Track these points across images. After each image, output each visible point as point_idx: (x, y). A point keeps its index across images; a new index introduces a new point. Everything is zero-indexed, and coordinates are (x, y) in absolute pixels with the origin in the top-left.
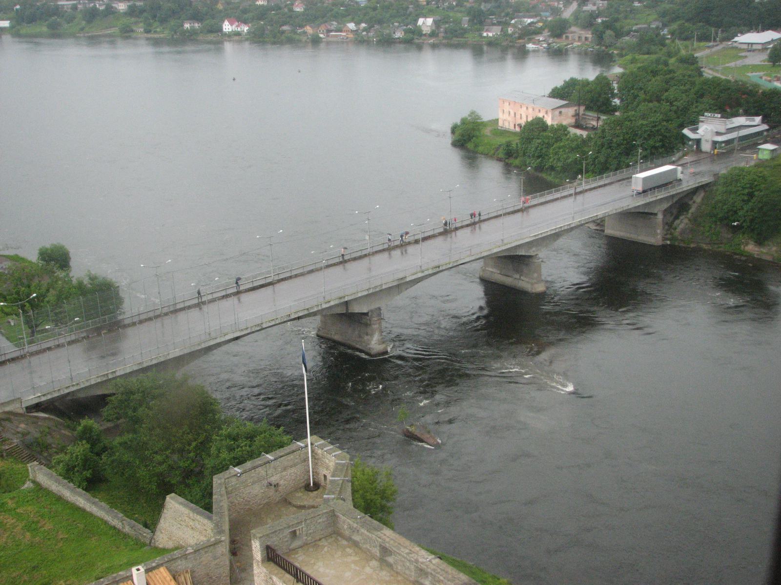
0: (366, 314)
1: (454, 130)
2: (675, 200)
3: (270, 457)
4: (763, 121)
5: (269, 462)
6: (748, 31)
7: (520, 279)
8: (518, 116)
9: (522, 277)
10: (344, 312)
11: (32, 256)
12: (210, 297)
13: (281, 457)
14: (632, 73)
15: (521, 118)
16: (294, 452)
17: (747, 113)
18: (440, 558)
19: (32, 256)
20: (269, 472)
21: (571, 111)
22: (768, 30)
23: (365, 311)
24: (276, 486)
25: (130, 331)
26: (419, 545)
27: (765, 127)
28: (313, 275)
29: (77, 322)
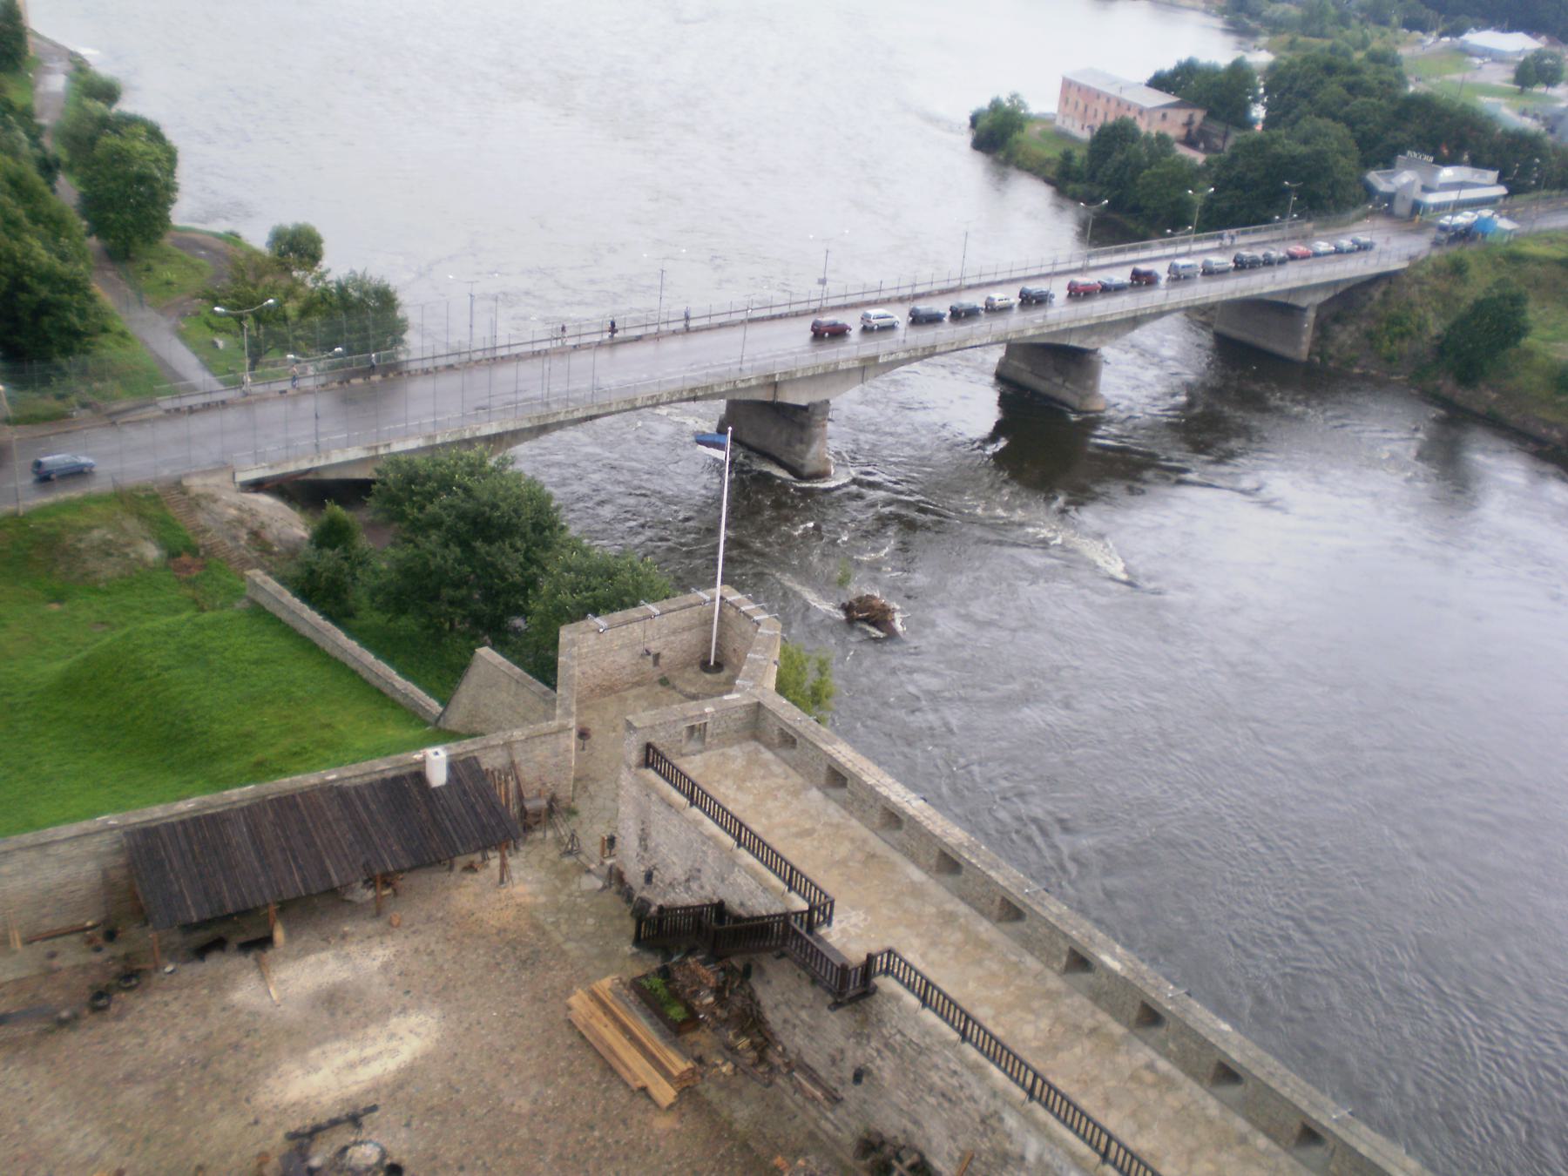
0: (805, 409)
1: (974, 120)
2: (1340, 289)
3: (653, 608)
4: (1500, 181)
5: (650, 617)
6: (1486, 27)
7: (1063, 386)
8: (1090, 112)
9: (1067, 384)
10: (771, 399)
11: (258, 238)
12: (705, 322)
13: (670, 611)
14: (1291, 65)
15: (1095, 116)
16: (691, 606)
17: (1475, 163)
18: (925, 800)
19: (258, 238)
20: (649, 633)
21: (1181, 116)
22: (1518, 30)
23: (803, 403)
24: (657, 657)
25: (418, 387)
26: (891, 774)
27: (1501, 190)
28: (723, 331)
29: (339, 355)
